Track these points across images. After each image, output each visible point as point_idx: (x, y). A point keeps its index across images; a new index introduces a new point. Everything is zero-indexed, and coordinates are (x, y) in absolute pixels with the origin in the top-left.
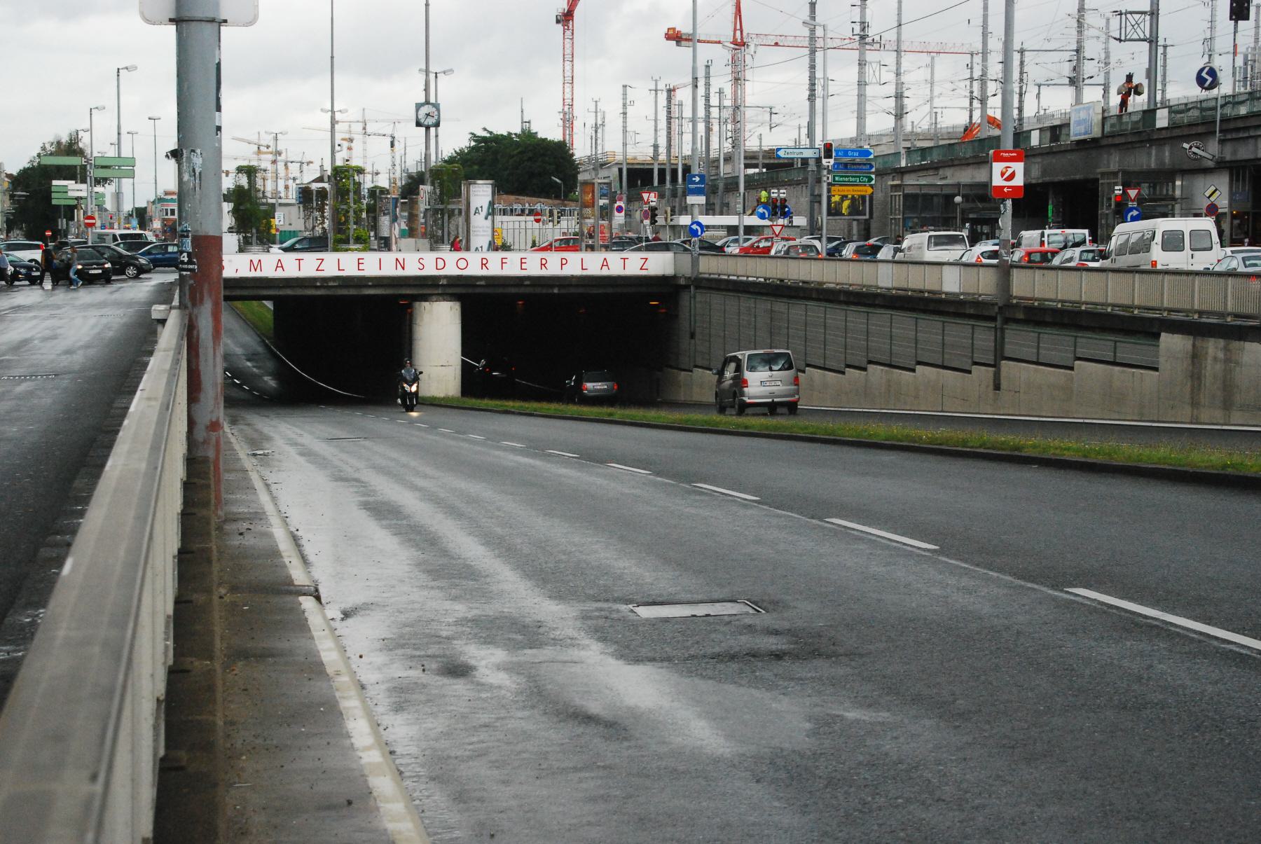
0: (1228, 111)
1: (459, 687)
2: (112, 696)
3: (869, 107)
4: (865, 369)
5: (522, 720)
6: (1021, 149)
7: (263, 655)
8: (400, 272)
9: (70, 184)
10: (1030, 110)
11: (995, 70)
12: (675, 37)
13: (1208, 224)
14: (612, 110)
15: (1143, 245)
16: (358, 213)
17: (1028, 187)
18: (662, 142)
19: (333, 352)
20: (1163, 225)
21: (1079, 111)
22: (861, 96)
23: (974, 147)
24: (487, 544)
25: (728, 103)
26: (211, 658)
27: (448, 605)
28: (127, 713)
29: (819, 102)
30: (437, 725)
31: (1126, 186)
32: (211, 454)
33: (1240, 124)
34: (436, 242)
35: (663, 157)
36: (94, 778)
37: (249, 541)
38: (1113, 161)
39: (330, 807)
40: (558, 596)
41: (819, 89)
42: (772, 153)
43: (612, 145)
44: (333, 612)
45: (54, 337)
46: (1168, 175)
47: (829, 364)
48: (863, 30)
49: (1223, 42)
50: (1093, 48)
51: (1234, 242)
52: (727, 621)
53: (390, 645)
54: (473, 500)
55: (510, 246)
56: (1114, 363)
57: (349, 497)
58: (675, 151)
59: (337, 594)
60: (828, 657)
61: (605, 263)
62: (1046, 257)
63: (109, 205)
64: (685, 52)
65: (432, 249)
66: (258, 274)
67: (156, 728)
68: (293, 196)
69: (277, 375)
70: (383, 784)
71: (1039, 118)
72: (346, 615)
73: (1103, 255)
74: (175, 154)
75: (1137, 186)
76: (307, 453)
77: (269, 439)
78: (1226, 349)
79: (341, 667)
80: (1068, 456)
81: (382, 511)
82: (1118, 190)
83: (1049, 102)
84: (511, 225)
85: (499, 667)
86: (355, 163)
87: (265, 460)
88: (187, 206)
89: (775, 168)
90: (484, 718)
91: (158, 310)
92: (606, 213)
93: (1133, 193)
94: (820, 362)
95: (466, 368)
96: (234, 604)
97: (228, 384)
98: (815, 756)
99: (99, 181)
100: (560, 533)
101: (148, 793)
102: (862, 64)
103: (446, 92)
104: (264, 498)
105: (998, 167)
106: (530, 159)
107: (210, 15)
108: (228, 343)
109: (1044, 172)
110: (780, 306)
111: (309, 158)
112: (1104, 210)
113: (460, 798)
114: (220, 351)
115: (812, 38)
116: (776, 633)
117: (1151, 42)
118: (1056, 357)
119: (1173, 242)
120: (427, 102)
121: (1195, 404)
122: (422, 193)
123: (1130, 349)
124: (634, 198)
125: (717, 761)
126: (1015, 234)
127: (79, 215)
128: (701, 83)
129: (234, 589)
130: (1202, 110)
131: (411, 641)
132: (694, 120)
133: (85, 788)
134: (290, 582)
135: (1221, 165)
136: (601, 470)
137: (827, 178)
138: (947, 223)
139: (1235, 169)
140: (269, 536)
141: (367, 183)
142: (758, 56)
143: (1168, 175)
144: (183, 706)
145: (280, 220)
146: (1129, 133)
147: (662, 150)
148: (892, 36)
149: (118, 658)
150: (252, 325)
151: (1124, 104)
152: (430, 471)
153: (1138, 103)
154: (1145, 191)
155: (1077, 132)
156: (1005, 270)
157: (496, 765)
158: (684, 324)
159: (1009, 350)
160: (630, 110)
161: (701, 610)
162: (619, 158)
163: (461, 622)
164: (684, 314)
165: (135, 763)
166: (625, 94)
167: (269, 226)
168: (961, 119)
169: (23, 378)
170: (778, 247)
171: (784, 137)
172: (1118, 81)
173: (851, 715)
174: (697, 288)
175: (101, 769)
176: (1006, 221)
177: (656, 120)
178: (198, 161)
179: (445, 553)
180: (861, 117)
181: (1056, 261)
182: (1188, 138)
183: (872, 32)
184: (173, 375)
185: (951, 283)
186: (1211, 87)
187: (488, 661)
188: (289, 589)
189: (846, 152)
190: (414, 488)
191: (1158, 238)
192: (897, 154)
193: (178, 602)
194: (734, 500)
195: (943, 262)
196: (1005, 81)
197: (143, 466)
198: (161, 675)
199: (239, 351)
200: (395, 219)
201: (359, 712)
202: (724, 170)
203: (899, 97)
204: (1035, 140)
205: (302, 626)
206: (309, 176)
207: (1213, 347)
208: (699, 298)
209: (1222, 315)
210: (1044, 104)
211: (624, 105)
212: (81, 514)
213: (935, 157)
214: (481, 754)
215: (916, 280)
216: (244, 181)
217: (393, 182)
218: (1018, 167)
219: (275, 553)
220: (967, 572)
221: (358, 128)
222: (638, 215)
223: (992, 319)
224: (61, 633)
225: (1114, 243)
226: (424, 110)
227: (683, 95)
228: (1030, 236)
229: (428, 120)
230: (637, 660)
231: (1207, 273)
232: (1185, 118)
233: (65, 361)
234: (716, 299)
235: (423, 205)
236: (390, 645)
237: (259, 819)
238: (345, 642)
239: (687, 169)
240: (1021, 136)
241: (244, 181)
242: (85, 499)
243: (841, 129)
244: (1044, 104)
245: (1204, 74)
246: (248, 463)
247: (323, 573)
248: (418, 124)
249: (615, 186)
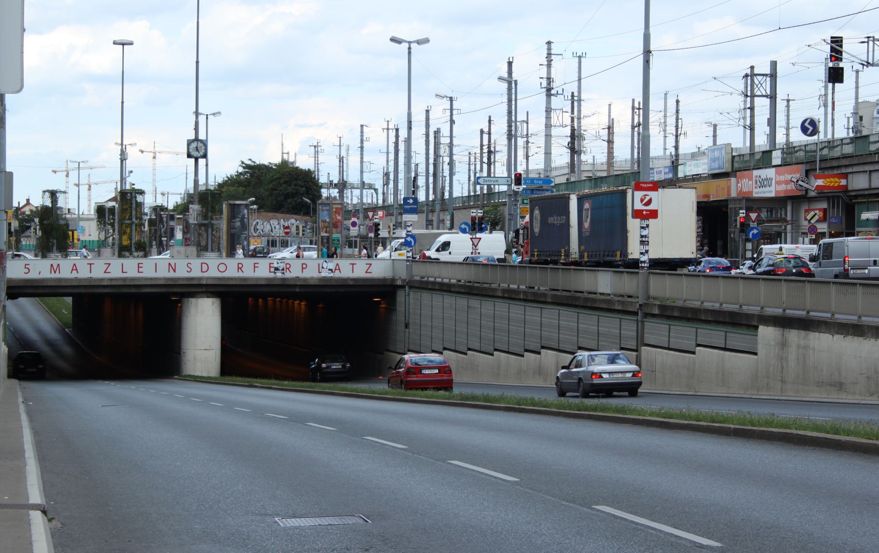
0: (825, 152)
4: (539, 353)
8: (172, 275)
21: (714, 151)
31: (749, 210)
33: (835, 164)
34: (201, 250)
48: (549, 84)
55: (296, 260)
56: (725, 349)
61: (75, 268)
65: (199, 256)
66: (57, 275)
68: (92, 213)
75: (758, 210)
82: (742, 213)
93: (753, 216)
94: (505, 348)
106: (286, 182)
110: (475, 302)
117: (771, 98)
120: (197, 139)
122: (191, 211)
123: (737, 338)
130: (806, 152)
135: (823, 194)
141: (149, 201)
150: (53, 311)
154: (764, 215)
158: (399, 316)
160: (365, 144)
164: (400, 308)
166: (362, 132)
174: (411, 287)
177: (388, 153)
186: (813, 134)
208: (412, 293)
211: (362, 141)
223: (635, 314)
229: (197, 150)
234: (426, 296)
245: (806, 124)
248: (189, 156)
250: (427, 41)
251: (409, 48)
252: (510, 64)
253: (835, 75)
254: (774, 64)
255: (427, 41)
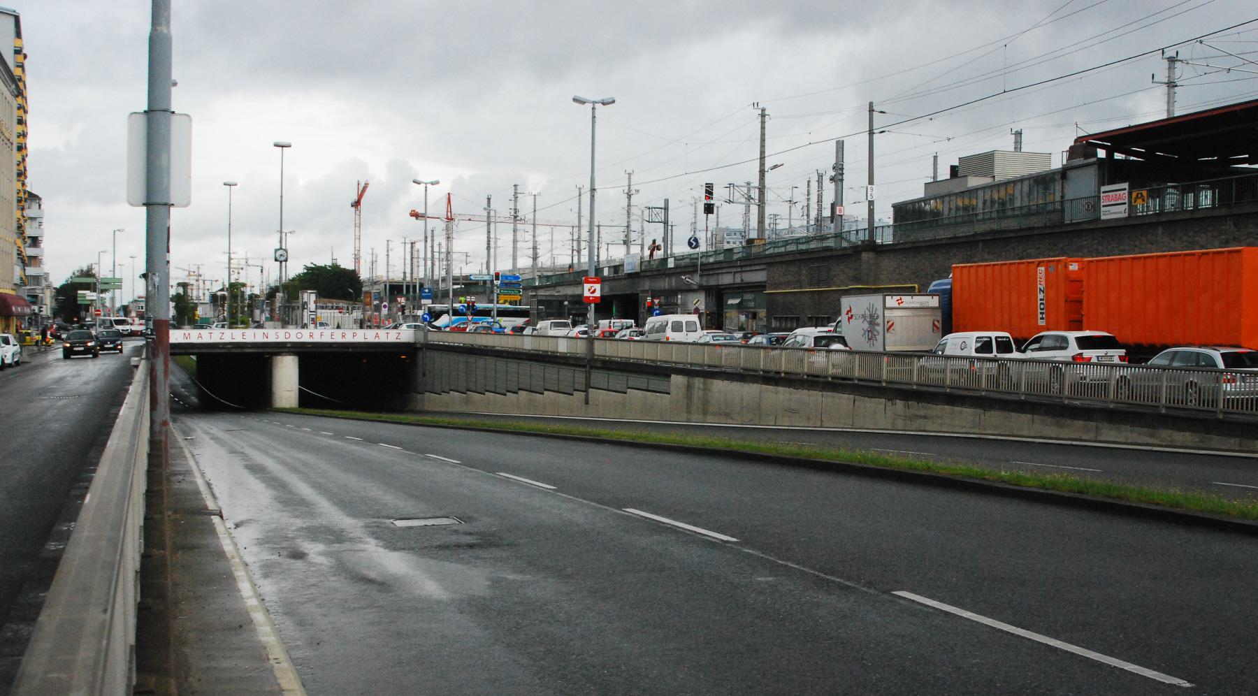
0: (704, 260)
1: (299, 564)
2: (113, 568)
3: (519, 253)
5: (334, 582)
6: (600, 279)
7: (192, 548)
8: (265, 340)
9: (87, 292)
10: (603, 257)
11: (585, 235)
12: (415, 215)
13: (694, 318)
14: (381, 255)
15: (662, 329)
16: (242, 308)
17: (602, 297)
18: (408, 271)
19: (230, 384)
20: (672, 318)
22: (515, 248)
23: (575, 276)
24: (313, 487)
25: (444, 250)
26: (164, 549)
27: (292, 520)
28: (121, 579)
29: (492, 251)
30: (287, 585)
32: (163, 438)
35: (408, 279)
36: (105, 611)
37: (184, 485)
38: (646, 285)
39: (230, 629)
40: (353, 514)
41: (492, 245)
42: (467, 277)
43: (381, 273)
44: (230, 524)
45: (78, 375)
46: (673, 292)
47: (562, 388)
49: (701, 225)
50: (635, 226)
51: (708, 328)
52: (445, 528)
53: (261, 542)
54: (305, 464)
55: (333, 328)
57: (238, 463)
58: (415, 276)
59: (233, 513)
60: (498, 546)
61: (377, 336)
62: (612, 334)
63: (108, 304)
64: (421, 223)
67: (135, 587)
68: (207, 299)
69: (197, 396)
70: (258, 617)
71: (608, 262)
72: (237, 526)
73: (642, 334)
74: (145, 276)
76: (214, 438)
77: (194, 431)
78: (704, 384)
79: (234, 553)
80: (623, 439)
81: (256, 470)
82: (649, 299)
83: (613, 253)
84: (324, 314)
85: (320, 554)
86: (241, 281)
87: (192, 442)
88: (151, 304)
89: (469, 286)
90: (313, 581)
91: (135, 360)
92: (378, 308)
93: (656, 301)
95: (301, 392)
96: (176, 520)
97: (172, 401)
98: (492, 599)
99: (103, 291)
100: (353, 481)
101: (132, 621)
102: (515, 231)
103: (292, 243)
104: (192, 463)
105: (587, 286)
107: (165, 201)
108: (172, 379)
109: (611, 289)
110: (472, 359)
111: (215, 279)
112: (642, 310)
113: (301, 623)
114: (168, 382)
115: (489, 217)
116: (470, 534)
118: (618, 388)
119: (677, 327)
121: (689, 412)
123: (656, 383)
124: (393, 300)
125: (439, 602)
126: (596, 321)
127: (92, 310)
128: (429, 239)
129: (176, 512)
131: (272, 539)
132: (425, 259)
133: (102, 617)
134: (206, 507)
135: (701, 288)
136: (375, 447)
137: (497, 291)
138: (560, 316)
139: (708, 290)
140: (195, 483)
141: (248, 291)
142: (459, 225)
143: (673, 292)
144: (151, 575)
145: (200, 312)
146: (654, 270)
147: (408, 275)
148: (530, 216)
149: (116, 547)
150: (184, 368)
151: (651, 255)
152: (281, 447)
153: (659, 254)
155: (627, 269)
156: (591, 341)
157: (319, 606)
159: (593, 382)
161: (430, 522)
162: (385, 279)
163: (300, 529)
165: (125, 605)
167: (194, 315)
168: (568, 261)
169: (60, 398)
170: (471, 327)
171: (473, 269)
172: (648, 243)
173: (511, 577)
175: (108, 606)
176: (591, 315)
178: (157, 279)
179: (291, 492)
180: (515, 258)
181: (617, 336)
182: (684, 273)
183: (520, 214)
184: (142, 395)
185: (563, 347)
186: (697, 246)
187: (314, 549)
188: (205, 512)
189: (507, 277)
190: (274, 457)
191: (670, 325)
192: (534, 279)
193: (146, 519)
194: (447, 463)
195: (559, 336)
196: (591, 241)
197: (127, 444)
198: (138, 558)
199: (177, 383)
200: (262, 311)
201: (245, 578)
202: (441, 286)
203: (535, 248)
204: (606, 272)
205: (212, 531)
206: (216, 288)
207: (698, 382)
209: (684, 364)
210: (611, 253)
212: (94, 471)
213: (554, 280)
214: (312, 600)
215: (543, 346)
216: (181, 291)
217: (262, 291)
218: (598, 287)
219: (198, 493)
220: (572, 501)
221: (243, 262)
222: (395, 310)
223: (584, 366)
224: (86, 534)
225: (647, 328)
226: (279, 253)
227: (420, 246)
228: (604, 323)
229: (281, 258)
230: (395, 549)
231: (694, 344)
232: (683, 263)
233: (84, 389)
234: (438, 356)
235: (278, 304)
236: (261, 542)
237: (192, 635)
238: (236, 540)
239: (421, 285)
240: (598, 270)
241: (181, 291)
242: (96, 463)
243: (503, 265)
244: (611, 253)
246: (182, 443)
247: (223, 503)
249: (382, 294)
250: (437, 183)
251: (594, 109)
252: (489, 199)
253: (709, 209)
254: (667, 201)
255: (437, 183)
